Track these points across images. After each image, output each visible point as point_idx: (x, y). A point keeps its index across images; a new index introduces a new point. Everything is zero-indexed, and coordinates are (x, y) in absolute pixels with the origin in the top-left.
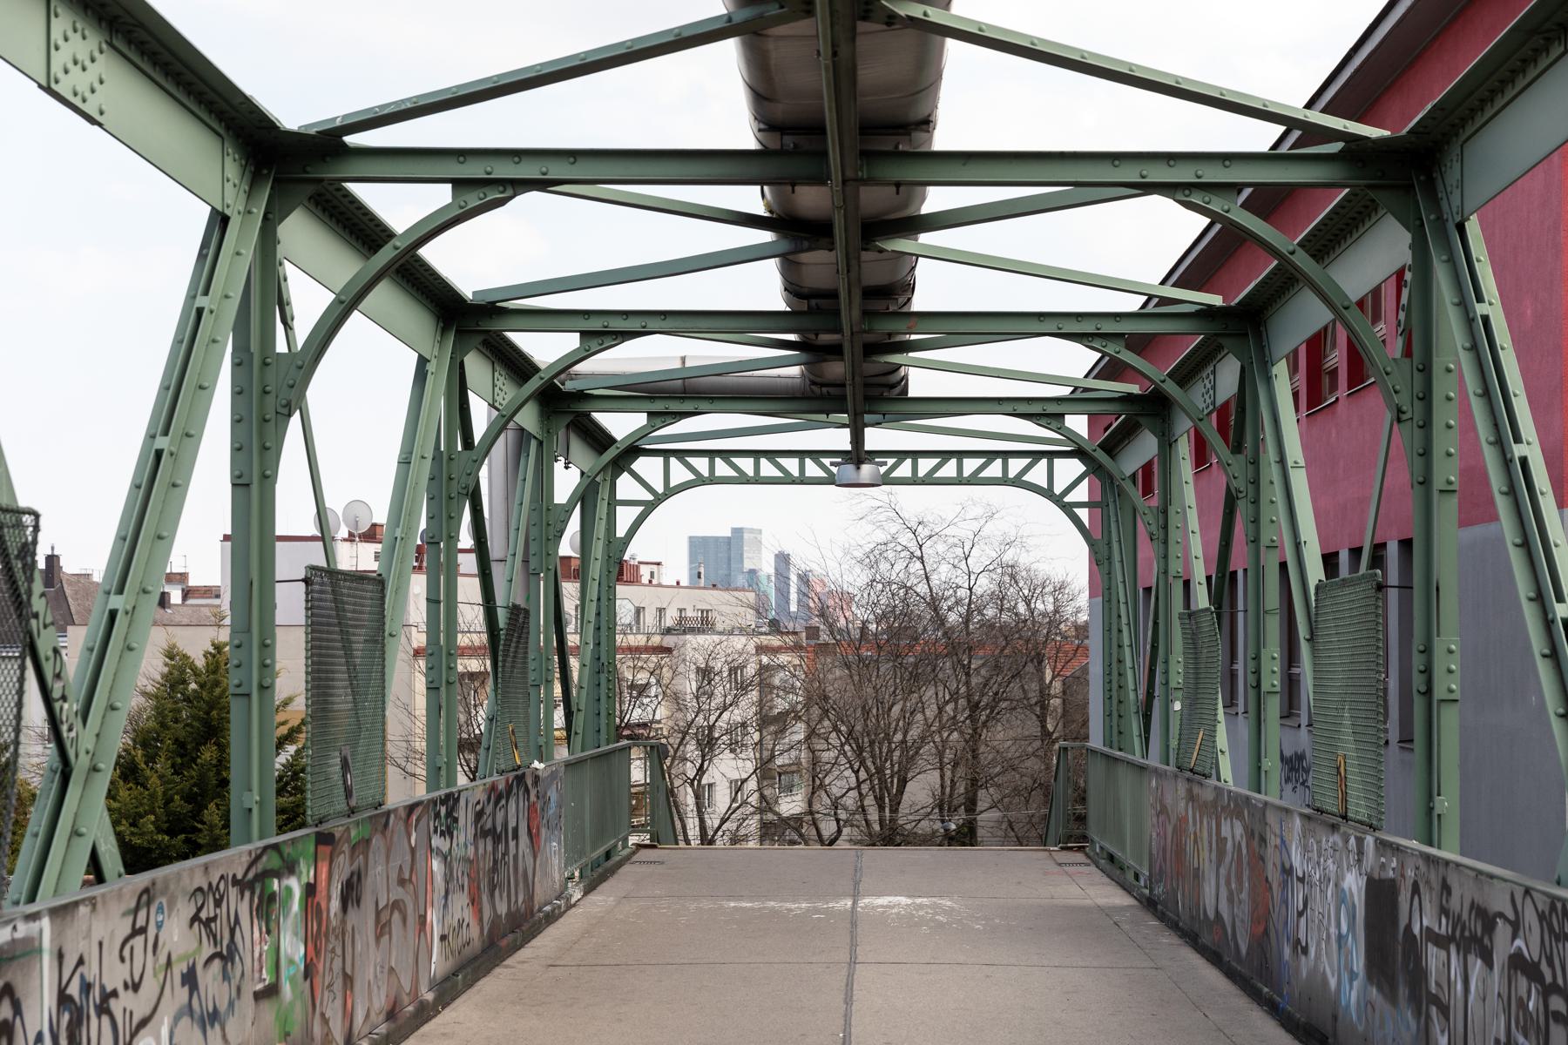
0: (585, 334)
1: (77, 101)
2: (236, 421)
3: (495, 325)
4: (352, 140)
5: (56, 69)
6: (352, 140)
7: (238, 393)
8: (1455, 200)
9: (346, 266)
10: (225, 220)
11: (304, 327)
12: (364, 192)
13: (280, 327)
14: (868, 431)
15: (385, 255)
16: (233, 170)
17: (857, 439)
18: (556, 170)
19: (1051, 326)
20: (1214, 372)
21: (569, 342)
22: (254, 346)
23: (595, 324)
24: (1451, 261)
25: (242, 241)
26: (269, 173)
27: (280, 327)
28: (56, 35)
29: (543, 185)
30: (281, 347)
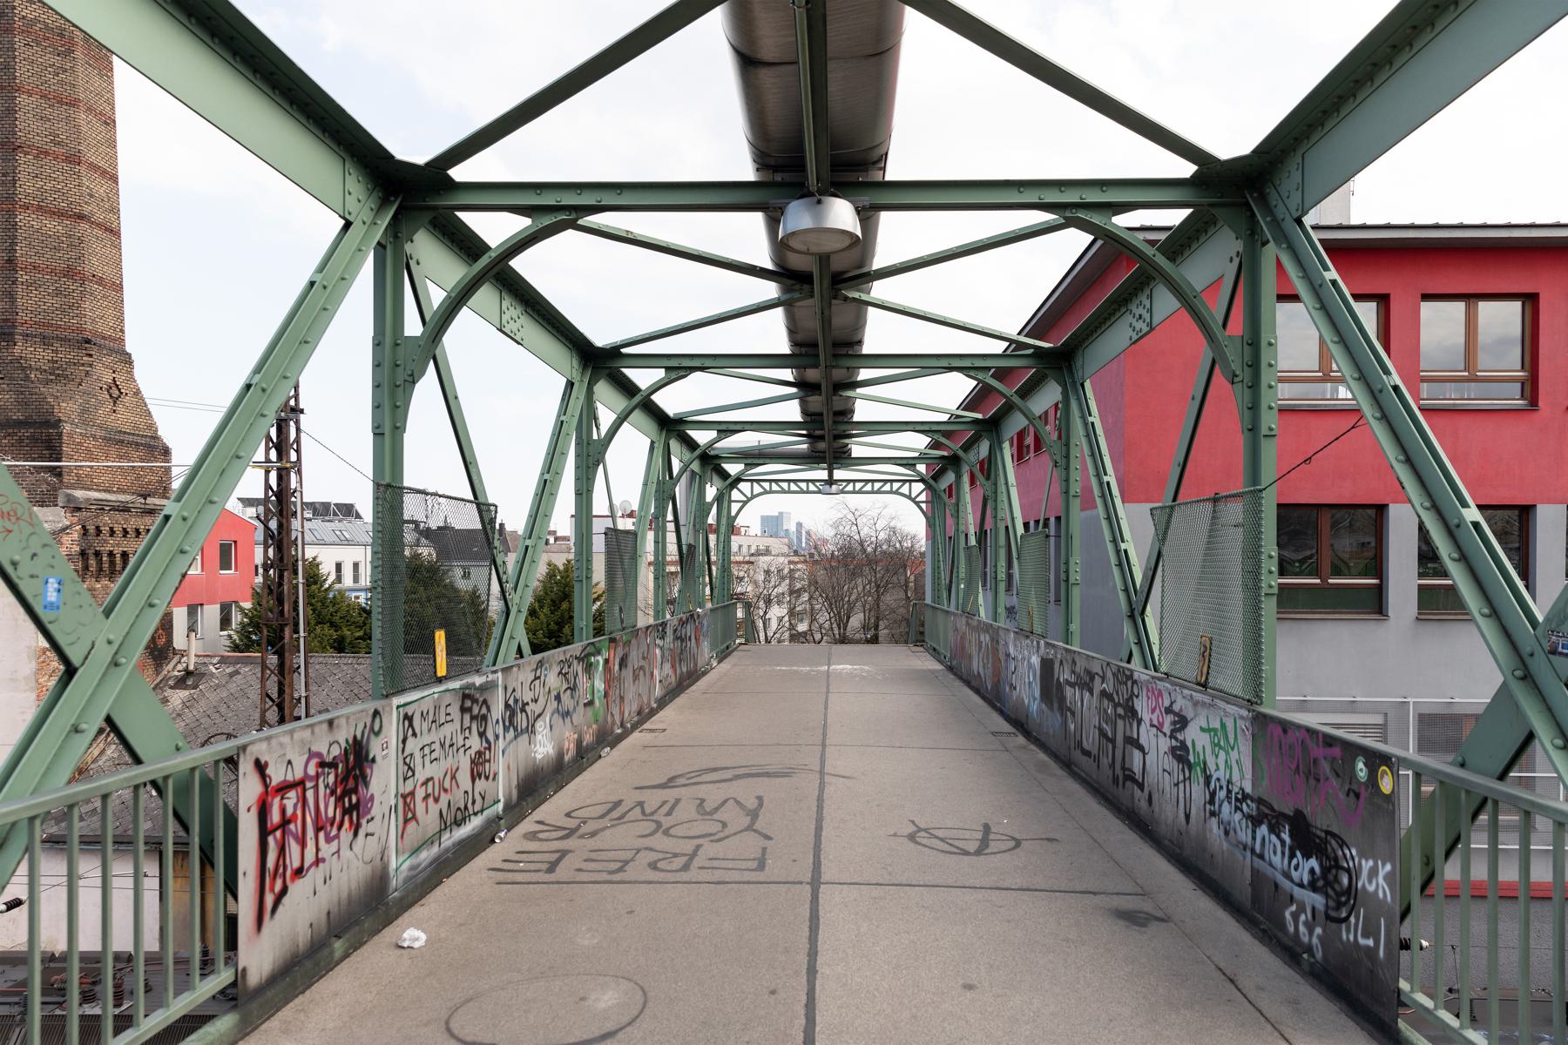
0: (719, 431)
1: (512, 335)
2: (577, 468)
3: (717, 462)
4: (624, 351)
5: (504, 322)
6: (624, 351)
7: (577, 456)
8: (1080, 373)
9: (621, 403)
10: (572, 384)
11: (604, 429)
12: (629, 372)
13: (595, 428)
14: (835, 471)
15: (638, 398)
16: (575, 363)
17: (831, 475)
18: (708, 363)
19: (911, 427)
20: (1150, 297)
21: (713, 434)
22: (584, 437)
23: (723, 427)
24: (1078, 399)
25: (579, 393)
26: (395, 201)
27: (595, 428)
28: (504, 308)
29: (702, 369)
30: (595, 437)
